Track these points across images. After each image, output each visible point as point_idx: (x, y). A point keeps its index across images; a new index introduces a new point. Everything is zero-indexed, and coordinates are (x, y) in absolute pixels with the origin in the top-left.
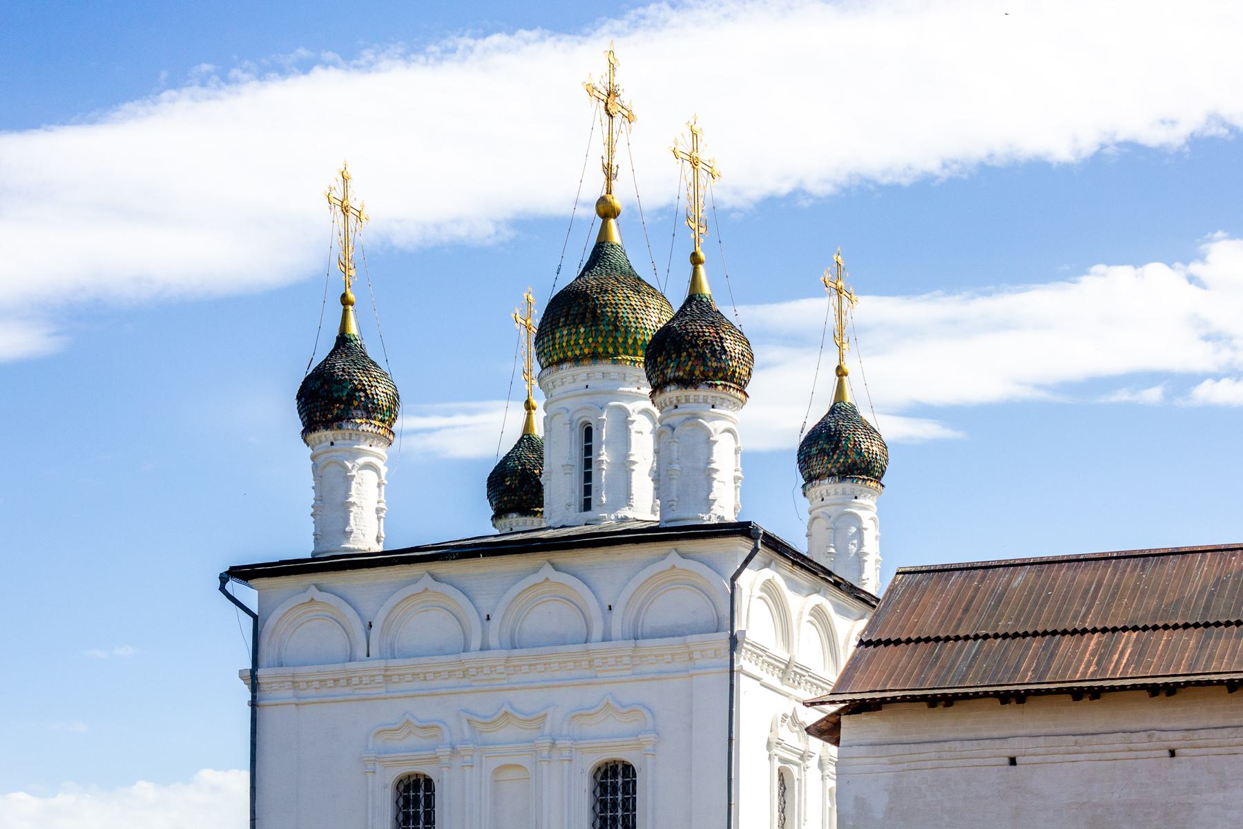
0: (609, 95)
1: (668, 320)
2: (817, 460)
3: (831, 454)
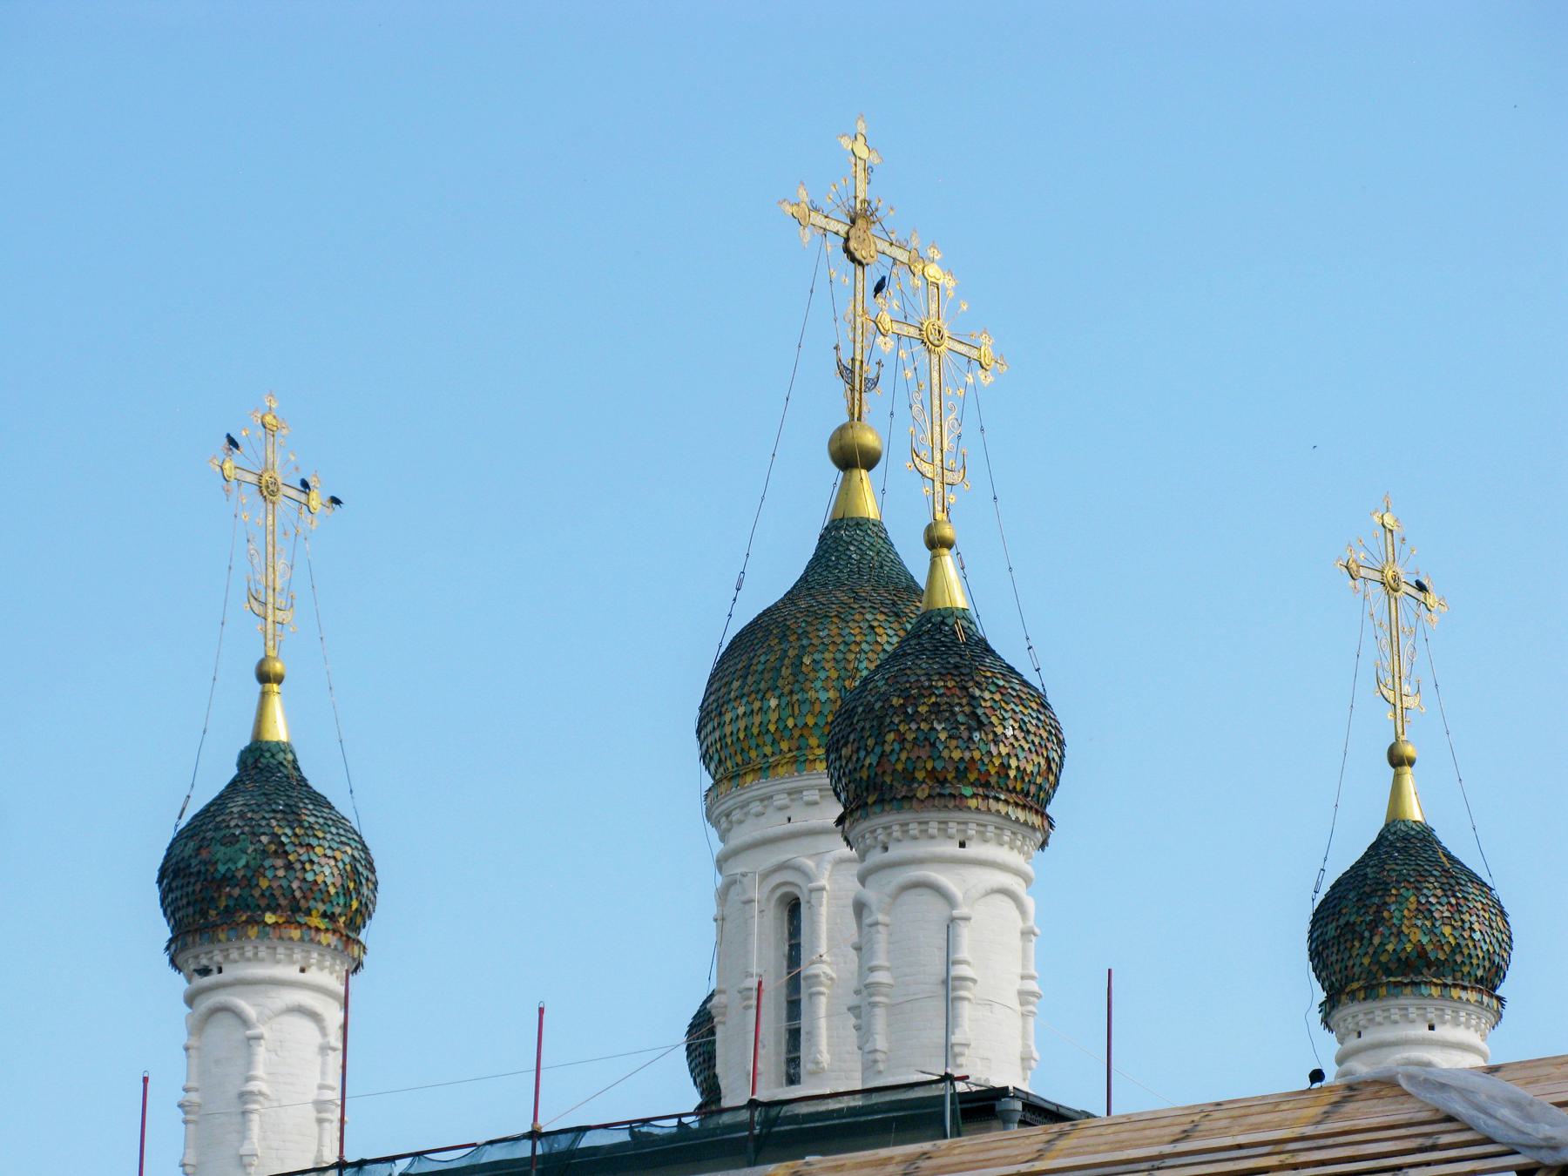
0: (853, 222)
1: (872, 667)
2: (1338, 950)
3: (1367, 934)
